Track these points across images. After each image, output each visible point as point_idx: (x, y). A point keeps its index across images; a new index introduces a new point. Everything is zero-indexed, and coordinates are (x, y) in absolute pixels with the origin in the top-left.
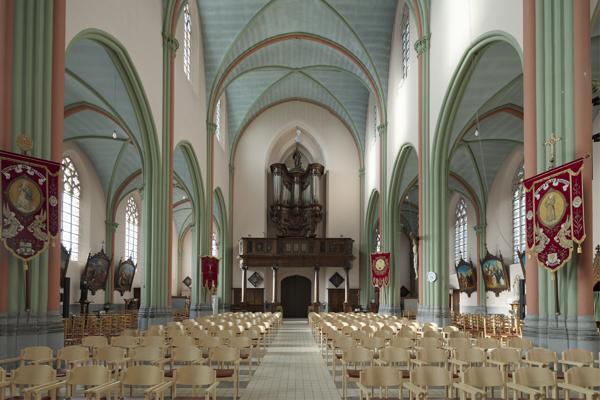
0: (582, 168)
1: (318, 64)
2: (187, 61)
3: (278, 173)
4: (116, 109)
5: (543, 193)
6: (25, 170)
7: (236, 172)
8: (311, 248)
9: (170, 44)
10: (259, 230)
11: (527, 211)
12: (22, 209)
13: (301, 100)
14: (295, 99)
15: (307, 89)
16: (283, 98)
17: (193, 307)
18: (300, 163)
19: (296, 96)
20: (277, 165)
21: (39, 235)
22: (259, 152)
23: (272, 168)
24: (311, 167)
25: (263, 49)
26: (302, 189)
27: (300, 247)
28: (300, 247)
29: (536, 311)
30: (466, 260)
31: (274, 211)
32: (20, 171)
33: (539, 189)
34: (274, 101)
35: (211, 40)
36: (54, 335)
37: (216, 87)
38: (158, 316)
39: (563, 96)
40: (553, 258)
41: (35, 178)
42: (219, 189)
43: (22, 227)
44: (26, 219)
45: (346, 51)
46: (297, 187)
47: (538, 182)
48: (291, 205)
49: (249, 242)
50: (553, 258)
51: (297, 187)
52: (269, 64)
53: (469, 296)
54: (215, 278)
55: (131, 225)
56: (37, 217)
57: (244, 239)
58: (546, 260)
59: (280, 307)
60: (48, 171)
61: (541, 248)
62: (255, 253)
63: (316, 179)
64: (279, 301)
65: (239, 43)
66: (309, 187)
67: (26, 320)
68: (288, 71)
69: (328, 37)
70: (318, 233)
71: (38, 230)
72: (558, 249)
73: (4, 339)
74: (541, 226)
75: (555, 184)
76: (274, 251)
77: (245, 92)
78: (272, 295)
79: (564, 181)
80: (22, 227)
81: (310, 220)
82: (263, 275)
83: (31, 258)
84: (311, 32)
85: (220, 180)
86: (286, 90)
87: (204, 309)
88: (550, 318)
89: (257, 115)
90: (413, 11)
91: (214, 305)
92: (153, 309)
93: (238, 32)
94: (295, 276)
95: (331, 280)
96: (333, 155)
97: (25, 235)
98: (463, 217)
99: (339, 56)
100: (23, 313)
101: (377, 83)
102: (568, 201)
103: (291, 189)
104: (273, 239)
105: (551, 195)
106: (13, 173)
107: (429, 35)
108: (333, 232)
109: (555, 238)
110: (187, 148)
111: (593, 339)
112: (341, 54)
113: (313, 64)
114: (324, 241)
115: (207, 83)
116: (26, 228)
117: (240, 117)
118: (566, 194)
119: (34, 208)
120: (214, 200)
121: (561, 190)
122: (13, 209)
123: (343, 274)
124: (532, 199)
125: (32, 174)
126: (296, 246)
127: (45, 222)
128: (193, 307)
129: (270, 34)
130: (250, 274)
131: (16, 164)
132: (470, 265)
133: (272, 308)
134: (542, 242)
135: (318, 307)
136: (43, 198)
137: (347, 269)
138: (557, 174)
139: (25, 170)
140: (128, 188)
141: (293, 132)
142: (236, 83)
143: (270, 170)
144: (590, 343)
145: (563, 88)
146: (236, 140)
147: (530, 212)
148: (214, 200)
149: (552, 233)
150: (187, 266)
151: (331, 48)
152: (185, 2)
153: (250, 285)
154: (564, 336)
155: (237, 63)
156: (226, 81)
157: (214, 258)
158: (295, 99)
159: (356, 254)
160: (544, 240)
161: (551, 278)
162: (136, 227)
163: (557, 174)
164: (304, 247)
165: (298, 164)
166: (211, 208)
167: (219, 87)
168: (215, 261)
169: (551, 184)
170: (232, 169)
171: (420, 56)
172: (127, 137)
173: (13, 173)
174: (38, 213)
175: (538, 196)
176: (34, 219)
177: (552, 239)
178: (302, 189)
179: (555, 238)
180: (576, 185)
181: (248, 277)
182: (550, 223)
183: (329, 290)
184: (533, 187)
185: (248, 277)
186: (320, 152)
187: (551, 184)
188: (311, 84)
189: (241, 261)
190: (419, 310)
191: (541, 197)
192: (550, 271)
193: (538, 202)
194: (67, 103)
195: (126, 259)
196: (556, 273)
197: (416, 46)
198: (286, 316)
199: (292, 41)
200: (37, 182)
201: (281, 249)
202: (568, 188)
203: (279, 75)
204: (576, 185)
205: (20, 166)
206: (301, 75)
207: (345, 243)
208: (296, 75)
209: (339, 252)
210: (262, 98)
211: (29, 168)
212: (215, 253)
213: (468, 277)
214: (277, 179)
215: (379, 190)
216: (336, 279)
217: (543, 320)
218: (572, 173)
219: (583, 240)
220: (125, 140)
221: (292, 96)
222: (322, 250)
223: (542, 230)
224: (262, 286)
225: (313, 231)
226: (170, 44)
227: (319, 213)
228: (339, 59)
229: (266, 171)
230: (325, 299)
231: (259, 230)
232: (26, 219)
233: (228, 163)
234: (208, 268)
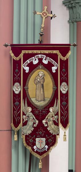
5: (32, 67)
11: (67, 94)
21: (51, 128)
33: (28, 61)
56: (51, 110)
58: (34, 144)
61: (28, 130)
71: (51, 123)
74: (30, 104)
75: (45, 62)
79: (54, 62)
105: (41, 72)
106: (31, 65)
121: (50, 71)
122: (30, 104)
134: (30, 123)
138: (47, 52)
160: (32, 122)
163: (47, 52)
169: (40, 60)
173: (31, 65)
175: (27, 69)
179: (44, 121)
180: (64, 70)
184: (21, 56)
191: (31, 70)
193: (26, 76)
202: (57, 70)
204: (64, 70)
219: (18, 128)
223: (30, 109)
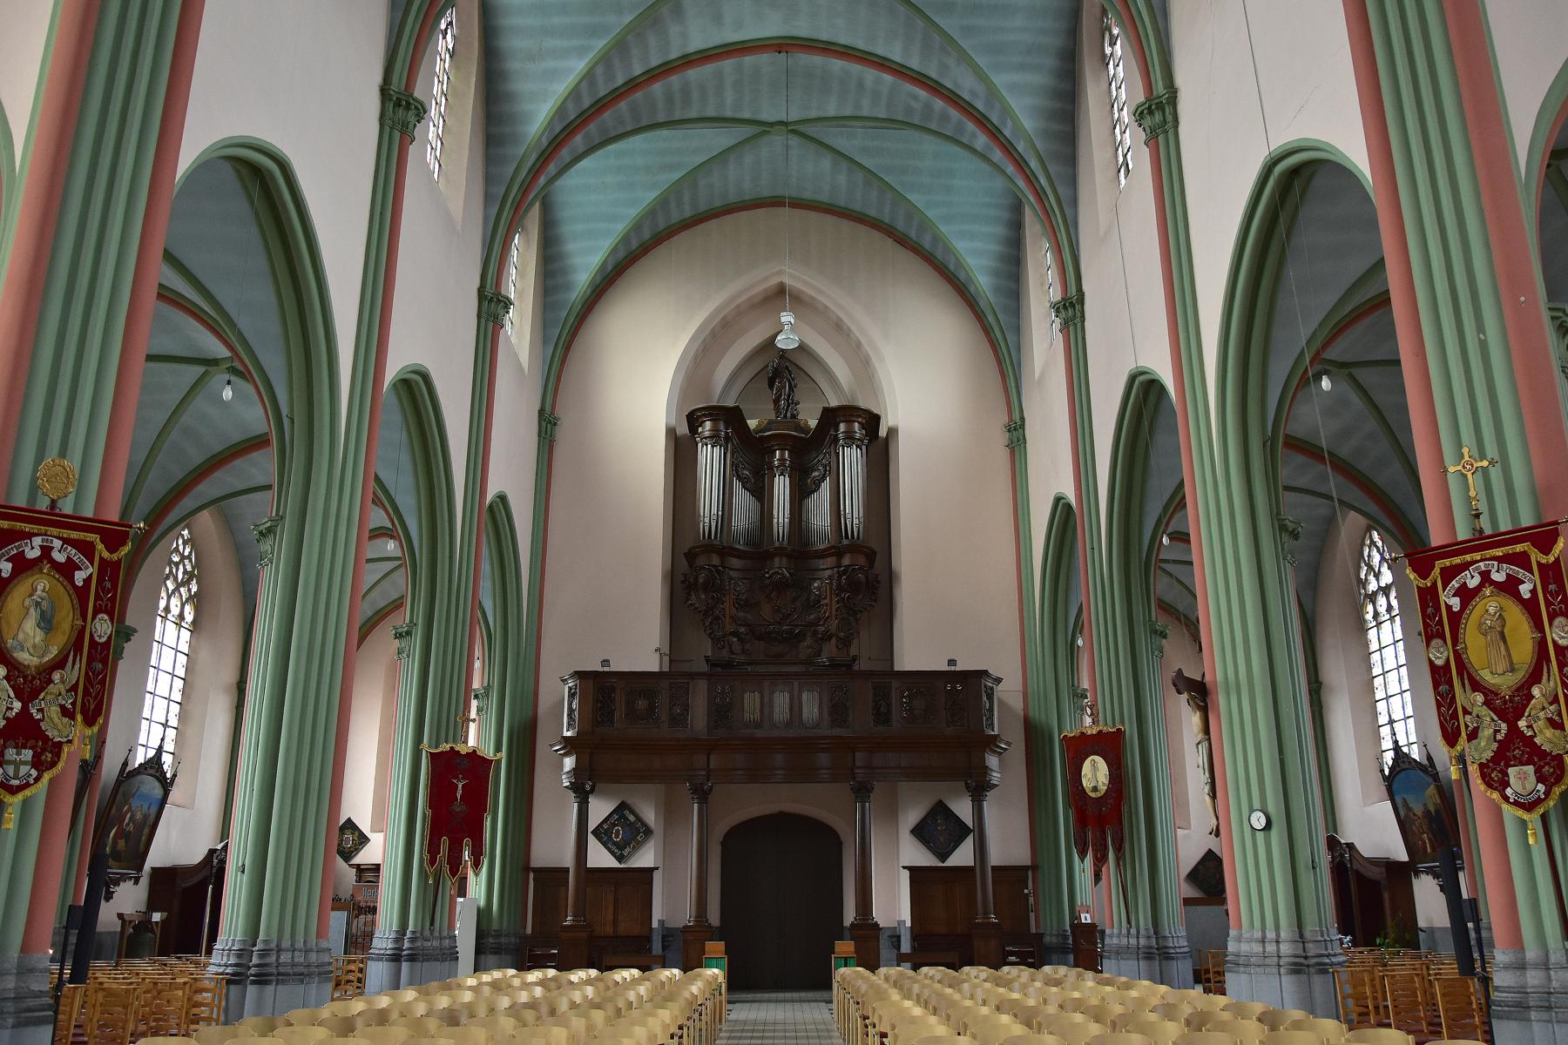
0: (1560, 544)
1: (848, 112)
2: (443, 144)
3: (715, 438)
4: (220, 296)
6: (46, 550)
7: (563, 435)
8: (837, 711)
9: (400, 109)
10: (640, 646)
12: (24, 657)
13: (797, 204)
14: (775, 202)
15: (812, 173)
16: (732, 197)
17: (383, 940)
18: (792, 403)
19: (780, 192)
20: (715, 412)
22: (644, 376)
23: (694, 419)
24: (831, 416)
25: (675, 79)
26: (802, 492)
27: (795, 707)
28: (795, 707)
29: (1517, 942)
30: (1415, 755)
31: (701, 571)
32: (36, 553)
33: (1455, 584)
34: (703, 207)
35: (514, 65)
36: (29, 1031)
37: (517, 189)
38: (282, 977)
39: (1483, 346)
40: (1522, 779)
41: (67, 569)
42: (502, 498)
43: (17, 705)
44: (28, 685)
45: (935, 88)
46: (781, 486)
47: (1447, 562)
48: (759, 547)
49: (601, 690)
50: (1522, 779)
51: (781, 486)
52: (693, 114)
53: (120, 916)
54: (475, 832)
55: (171, 627)
56: (56, 676)
57: (579, 675)
59: (716, 947)
60: (100, 546)
61: (1484, 748)
62: (621, 726)
63: (852, 460)
64: (714, 918)
65: (599, 71)
66: (826, 487)
67: (290, 955)
68: (748, 131)
69: (880, 51)
70: (864, 653)
71: (54, 711)
72: (1534, 754)
73: (7, 1033)
74: (1477, 686)
76: (699, 718)
77: (602, 199)
78: (676, 883)
79: (1521, 573)
80: (17, 705)
81: (830, 605)
82: (650, 815)
83: (27, 792)
84: (824, 37)
85: (510, 474)
86: (740, 178)
87: (423, 955)
88: (1553, 959)
89: (645, 250)
90: (1119, 15)
91: (465, 934)
92: (264, 953)
93: (600, 44)
94: (782, 816)
95: (919, 832)
96: (916, 377)
97: (24, 730)
98: (1385, 590)
99: (915, 98)
100: (427, 933)
101: (1043, 180)
102: (1538, 626)
103: (761, 492)
104: (693, 676)
105: (1490, 604)
107: (1023, 419)
108: (918, 647)
109: (1522, 724)
110: (416, 392)
111: (1297, 972)
112: (923, 94)
113: (831, 112)
114: (888, 680)
115: (489, 179)
116: (25, 709)
117: (586, 260)
118: (1530, 606)
119: (54, 651)
120: (485, 551)
121: (1516, 595)
123: (963, 809)
124: (1438, 609)
125: (60, 557)
126: (781, 701)
127: (74, 688)
128: (383, 940)
129: (697, 43)
130: (600, 809)
131: (30, 536)
132: (1428, 768)
133: (684, 950)
134: (1486, 733)
135: (870, 946)
136: (80, 622)
137: (979, 788)
139: (46, 550)
140: (187, 503)
141: (779, 296)
142: (571, 180)
143: (683, 429)
144: (1293, 977)
145: (1480, 328)
146: (568, 329)
147: (1436, 642)
148: (485, 551)
149: (1510, 708)
150: (373, 786)
151: (888, 78)
152: (450, 2)
153: (599, 857)
154: (1275, 970)
155: (588, 122)
156: (552, 168)
157: (473, 755)
158: (775, 202)
159: (1005, 725)
160: (1491, 729)
161: (1535, 841)
162: (185, 635)
163: (1499, 552)
164: (811, 707)
165: (786, 405)
166: (457, 566)
167: (526, 189)
168: (477, 765)
169: (1485, 576)
170: (548, 423)
171: (1152, 140)
172: (223, 352)
174: (59, 663)
175: (1455, 603)
176: (50, 681)
177: (1513, 728)
178: (802, 492)
179: (1522, 724)
180: (1552, 587)
181: (593, 824)
182: (1503, 681)
183: (918, 875)
185: (593, 824)
186: (863, 366)
187: (1485, 576)
188: (826, 163)
189: (569, 763)
190: (1232, 947)
191: (1464, 605)
192: (1533, 818)
193: (1456, 618)
194: (372, 526)
195: (140, 758)
196: (1544, 818)
197: (1140, 115)
198: (741, 982)
199: (765, 58)
200: (71, 579)
201: (721, 713)
203: (720, 139)
205: (37, 541)
206: (794, 141)
207: (963, 690)
208: (777, 140)
209: (945, 724)
210: (663, 203)
211: (57, 543)
212: (475, 738)
213: (1427, 813)
214: (710, 459)
215: (1072, 498)
216: (939, 830)
217: (1536, 966)
218: (1536, 556)
220: (213, 362)
221: (766, 193)
222: (882, 717)
223: (1480, 698)
224: (645, 858)
225: (846, 642)
226: (400, 109)
227: (864, 572)
228: (916, 105)
229: (671, 432)
230: (893, 905)
231: (640, 646)
232: (28, 685)
233: (537, 407)
234: (453, 802)
